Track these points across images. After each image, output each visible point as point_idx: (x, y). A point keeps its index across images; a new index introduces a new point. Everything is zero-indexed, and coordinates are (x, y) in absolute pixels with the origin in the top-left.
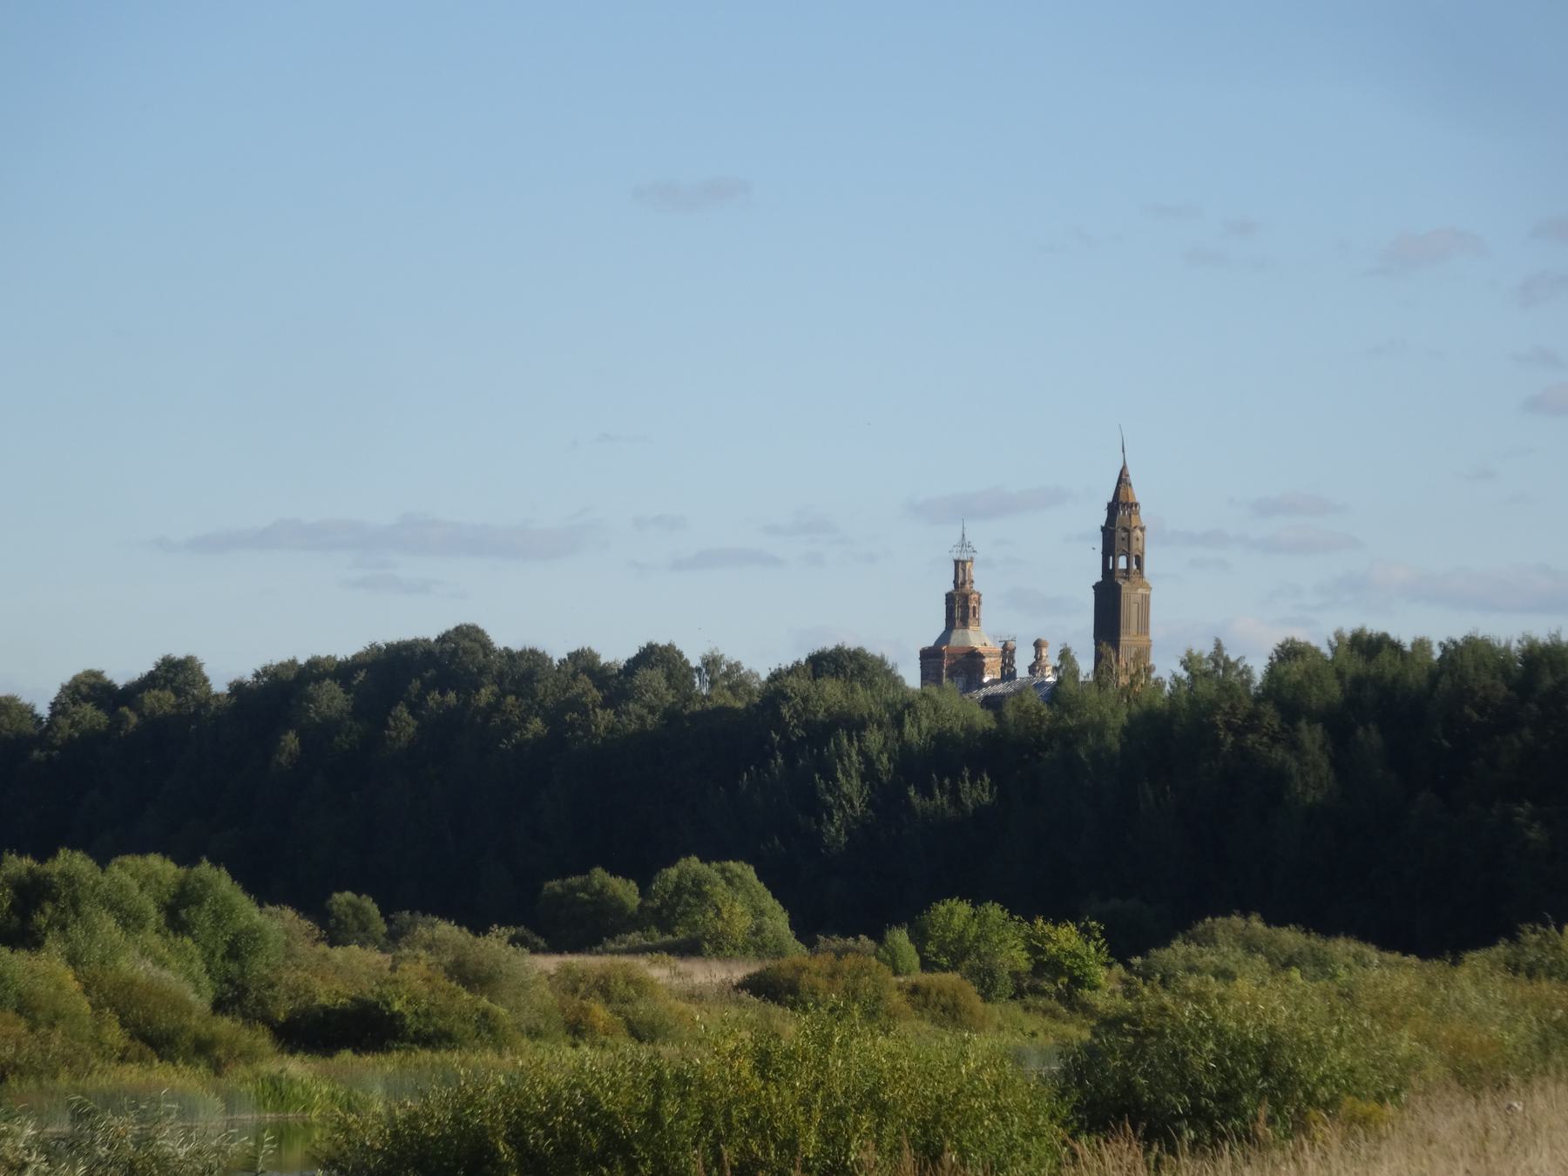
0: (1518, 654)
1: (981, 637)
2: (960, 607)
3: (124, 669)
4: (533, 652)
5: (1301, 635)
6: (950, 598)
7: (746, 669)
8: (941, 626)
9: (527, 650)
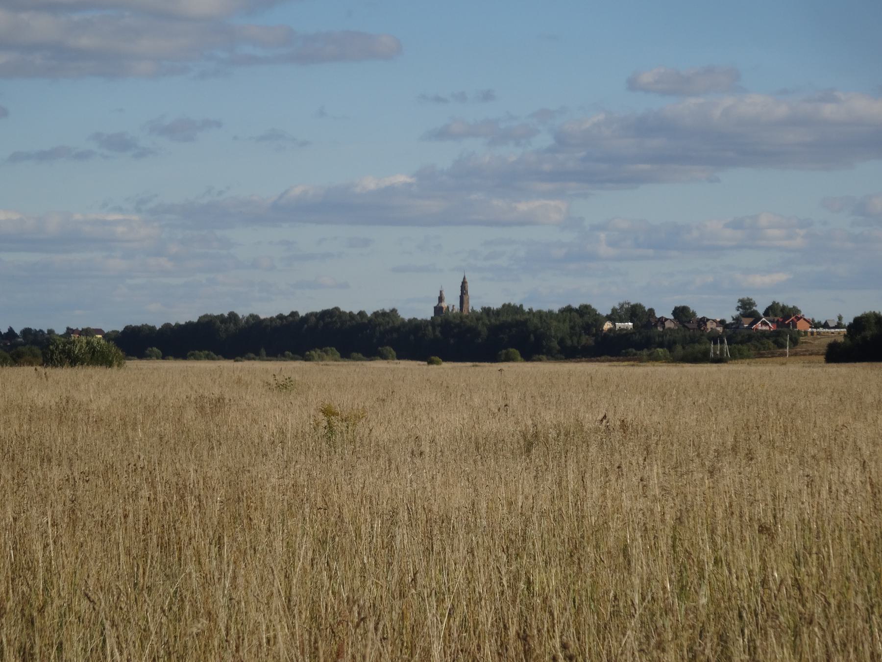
0: (470, 308)
1: (444, 305)
2: (441, 299)
3: (286, 313)
4: (165, 324)
5: (353, 311)
6: (439, 298)
7: (802, 314)
8: (438, 303)
9: (18, 331)
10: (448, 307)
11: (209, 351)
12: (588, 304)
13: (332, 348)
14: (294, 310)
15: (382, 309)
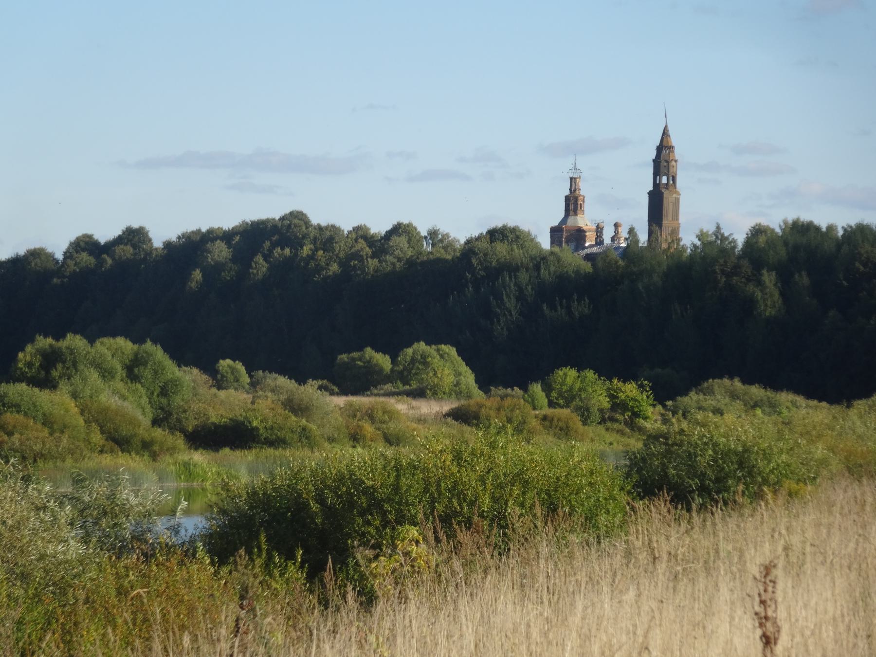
1: (585, 220)
2: (573, 204)
3: (105, 233)
5: (764, 222)
6: (567, 199)
8: (562, 214)
10: (599, 230)
11: (138, 340)
12: (37, 246)
13: (445, 348)
14: (135, 225)
15: (198, 228)
